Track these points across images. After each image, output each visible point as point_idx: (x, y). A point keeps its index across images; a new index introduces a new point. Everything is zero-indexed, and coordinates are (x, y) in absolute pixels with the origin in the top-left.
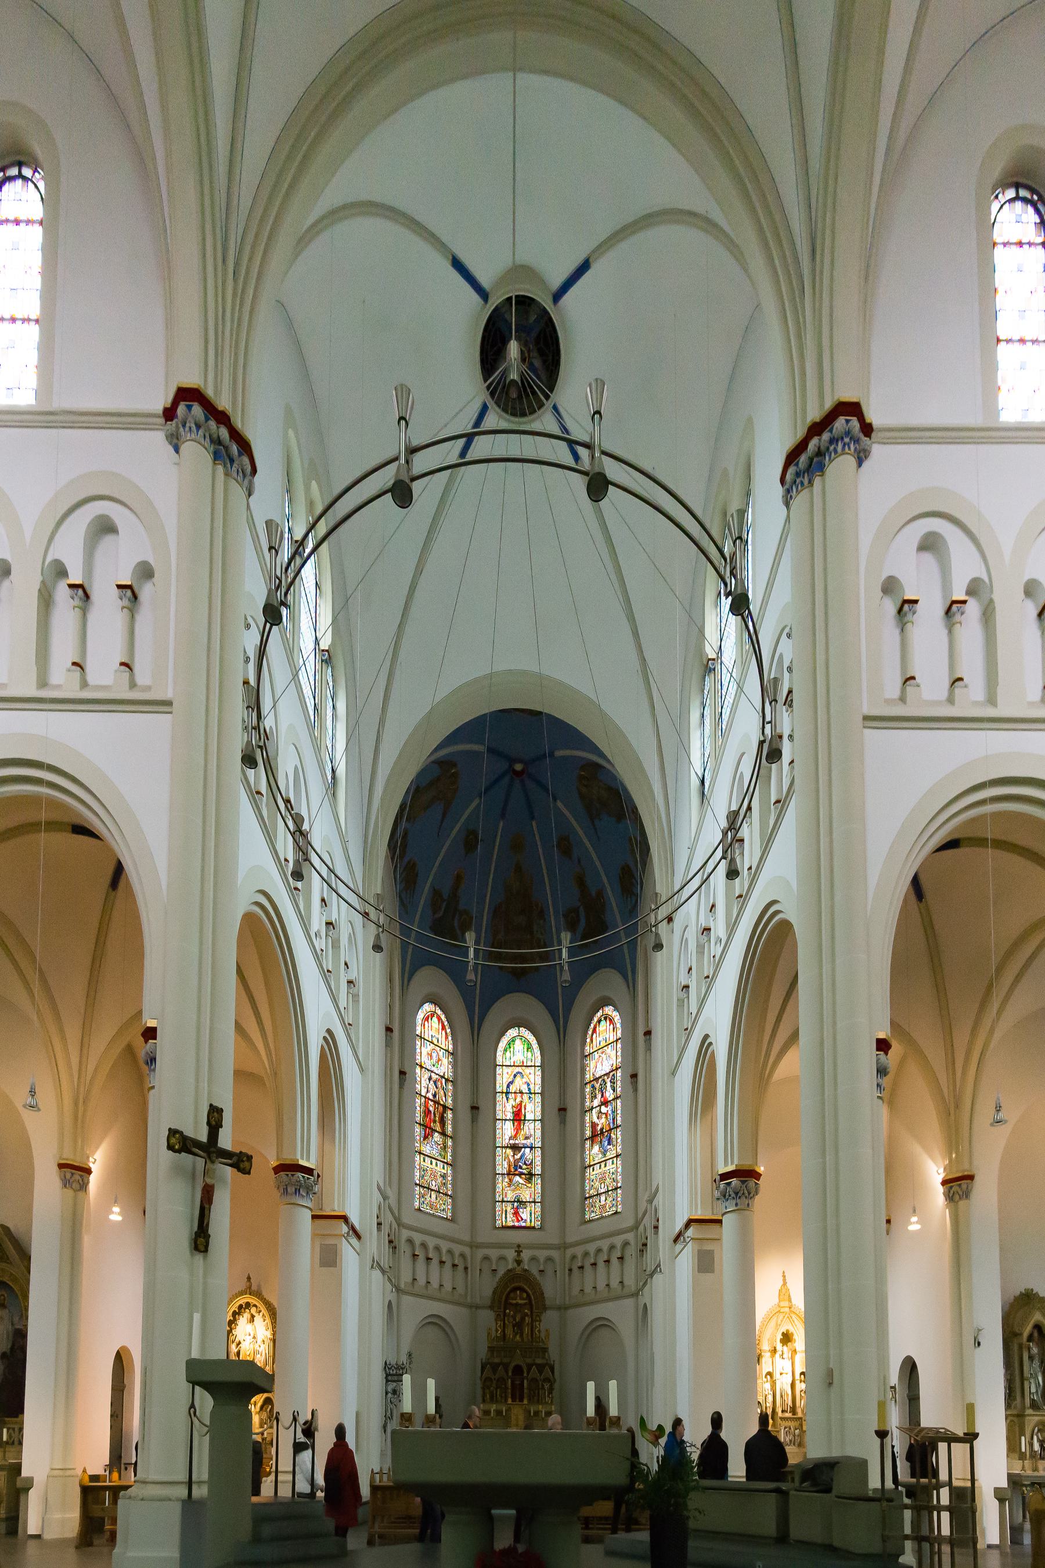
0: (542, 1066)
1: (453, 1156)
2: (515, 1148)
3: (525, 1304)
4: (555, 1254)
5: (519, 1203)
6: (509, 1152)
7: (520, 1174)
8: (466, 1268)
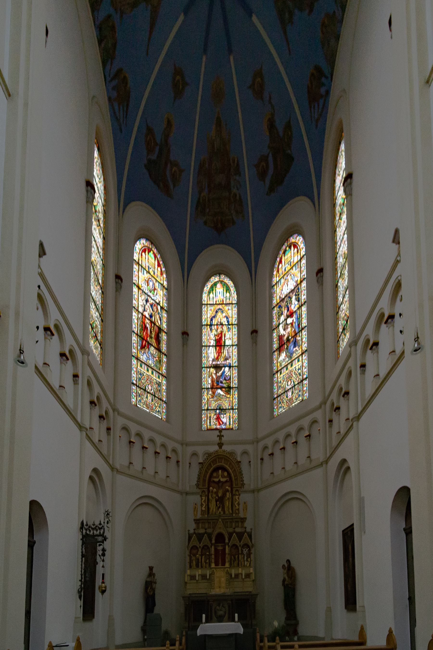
0: (238, 304)
1: (168, 369)
2: (217, 367)
3: (226, 481)
4: (250, 448)
5: (220, 411)
6: (213, 370)
7: (221, 388)
8: (178, 462)
